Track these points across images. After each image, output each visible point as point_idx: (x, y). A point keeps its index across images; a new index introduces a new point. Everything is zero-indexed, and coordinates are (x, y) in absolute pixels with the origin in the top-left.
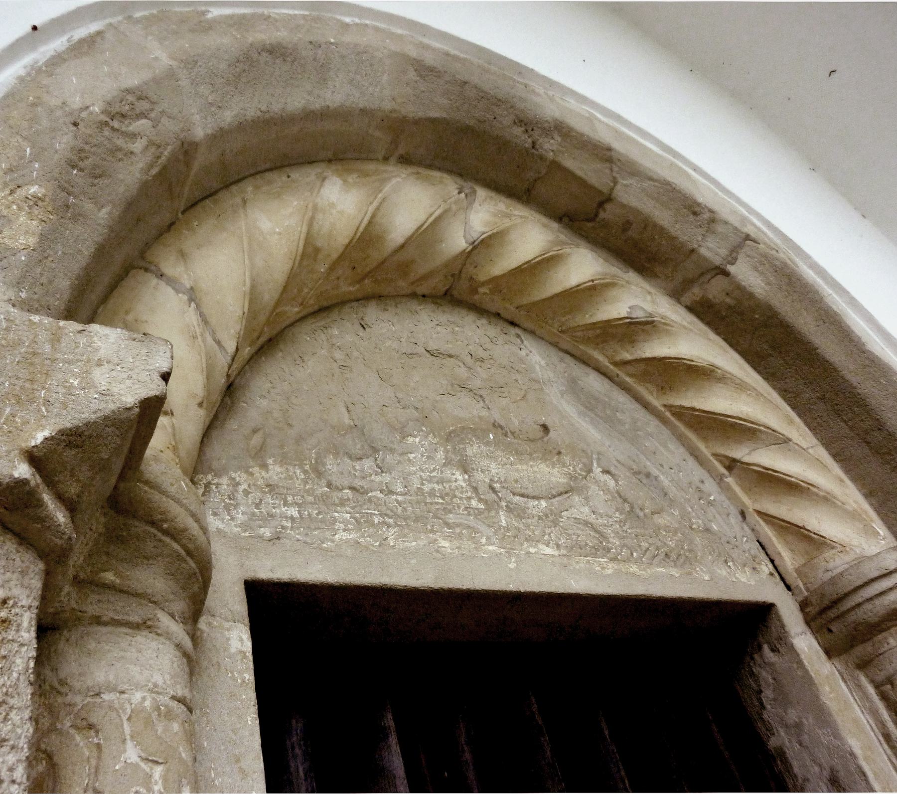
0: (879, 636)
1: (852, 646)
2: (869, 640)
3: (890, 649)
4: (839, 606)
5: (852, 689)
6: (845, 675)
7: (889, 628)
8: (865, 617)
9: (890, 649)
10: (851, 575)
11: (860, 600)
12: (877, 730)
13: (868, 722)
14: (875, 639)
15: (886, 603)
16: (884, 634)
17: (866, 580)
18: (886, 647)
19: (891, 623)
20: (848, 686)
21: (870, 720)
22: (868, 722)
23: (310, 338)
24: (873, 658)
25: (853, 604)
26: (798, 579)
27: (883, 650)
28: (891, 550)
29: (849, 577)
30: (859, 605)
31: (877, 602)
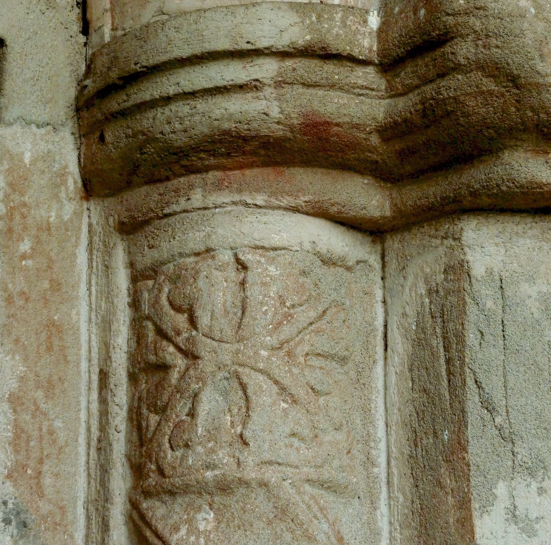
0: (182, 179)
1: (129, 185)
2: (160, 181)
3: (185, 211)
4: (132, 90)
5: (94, 270)
6: (96, 239)
7: (207, 169)
8: (167, 129)
9: (185, 211)
10: (177, 29)
11: (172, 90)
12: (95, 361)
13: (90, 341)
14: (175, 183)
15: (217, 113)
16: (192, 177)
17: (198, 50)
18: (183, 204)
19: (213, 161)
20: (90, 260)
21: (93, 337)
22: (90, 341)
23: (401, 13)
24: (151, 218)
25: (156, 94)
26: (109, 14)
27: (175, 208)
28: (284, 7)
29: (172, 33)
30: (167, 100)
31: (201, 105)
